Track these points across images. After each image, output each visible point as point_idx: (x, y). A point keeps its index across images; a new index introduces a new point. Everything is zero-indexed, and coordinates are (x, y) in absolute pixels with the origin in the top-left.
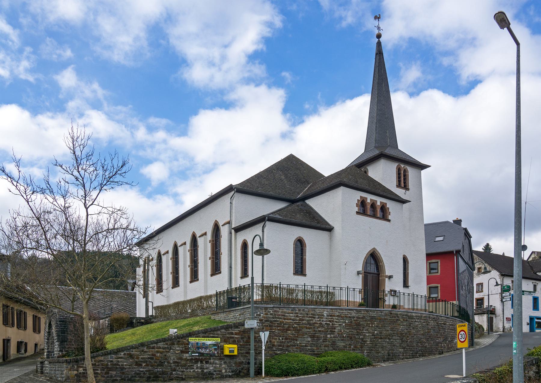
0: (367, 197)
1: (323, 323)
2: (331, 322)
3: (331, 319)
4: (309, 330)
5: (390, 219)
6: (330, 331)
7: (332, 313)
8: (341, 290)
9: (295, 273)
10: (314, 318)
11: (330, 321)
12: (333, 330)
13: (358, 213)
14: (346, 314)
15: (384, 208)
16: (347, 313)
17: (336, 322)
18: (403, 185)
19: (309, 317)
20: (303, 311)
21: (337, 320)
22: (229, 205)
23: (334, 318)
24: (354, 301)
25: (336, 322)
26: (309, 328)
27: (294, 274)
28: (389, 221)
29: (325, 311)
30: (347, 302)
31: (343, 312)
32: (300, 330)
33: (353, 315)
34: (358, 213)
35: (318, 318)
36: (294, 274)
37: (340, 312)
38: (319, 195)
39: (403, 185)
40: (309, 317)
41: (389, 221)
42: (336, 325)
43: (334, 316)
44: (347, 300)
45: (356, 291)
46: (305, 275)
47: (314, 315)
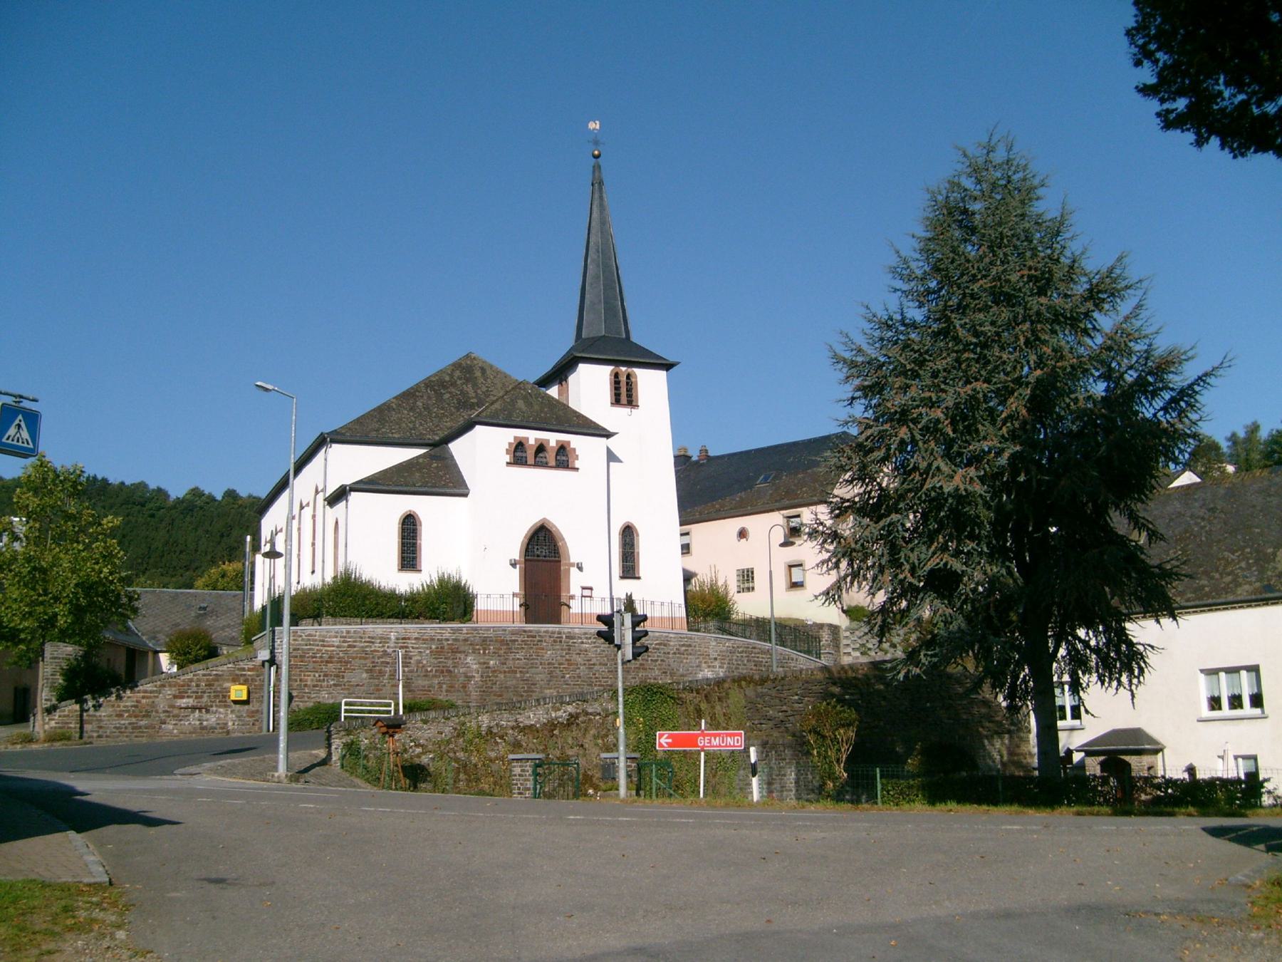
5: (576, 466)
10: (373, 643)
13: (508, 464)
15: (562, 448)
17: (413, 648)
18: (624, 399)
25: (413, 648)
26: (366, 659)
34: (508, 464)
35: (380, 643)
39: (624, 399)
41: (578, 469)
43: (409, 639)
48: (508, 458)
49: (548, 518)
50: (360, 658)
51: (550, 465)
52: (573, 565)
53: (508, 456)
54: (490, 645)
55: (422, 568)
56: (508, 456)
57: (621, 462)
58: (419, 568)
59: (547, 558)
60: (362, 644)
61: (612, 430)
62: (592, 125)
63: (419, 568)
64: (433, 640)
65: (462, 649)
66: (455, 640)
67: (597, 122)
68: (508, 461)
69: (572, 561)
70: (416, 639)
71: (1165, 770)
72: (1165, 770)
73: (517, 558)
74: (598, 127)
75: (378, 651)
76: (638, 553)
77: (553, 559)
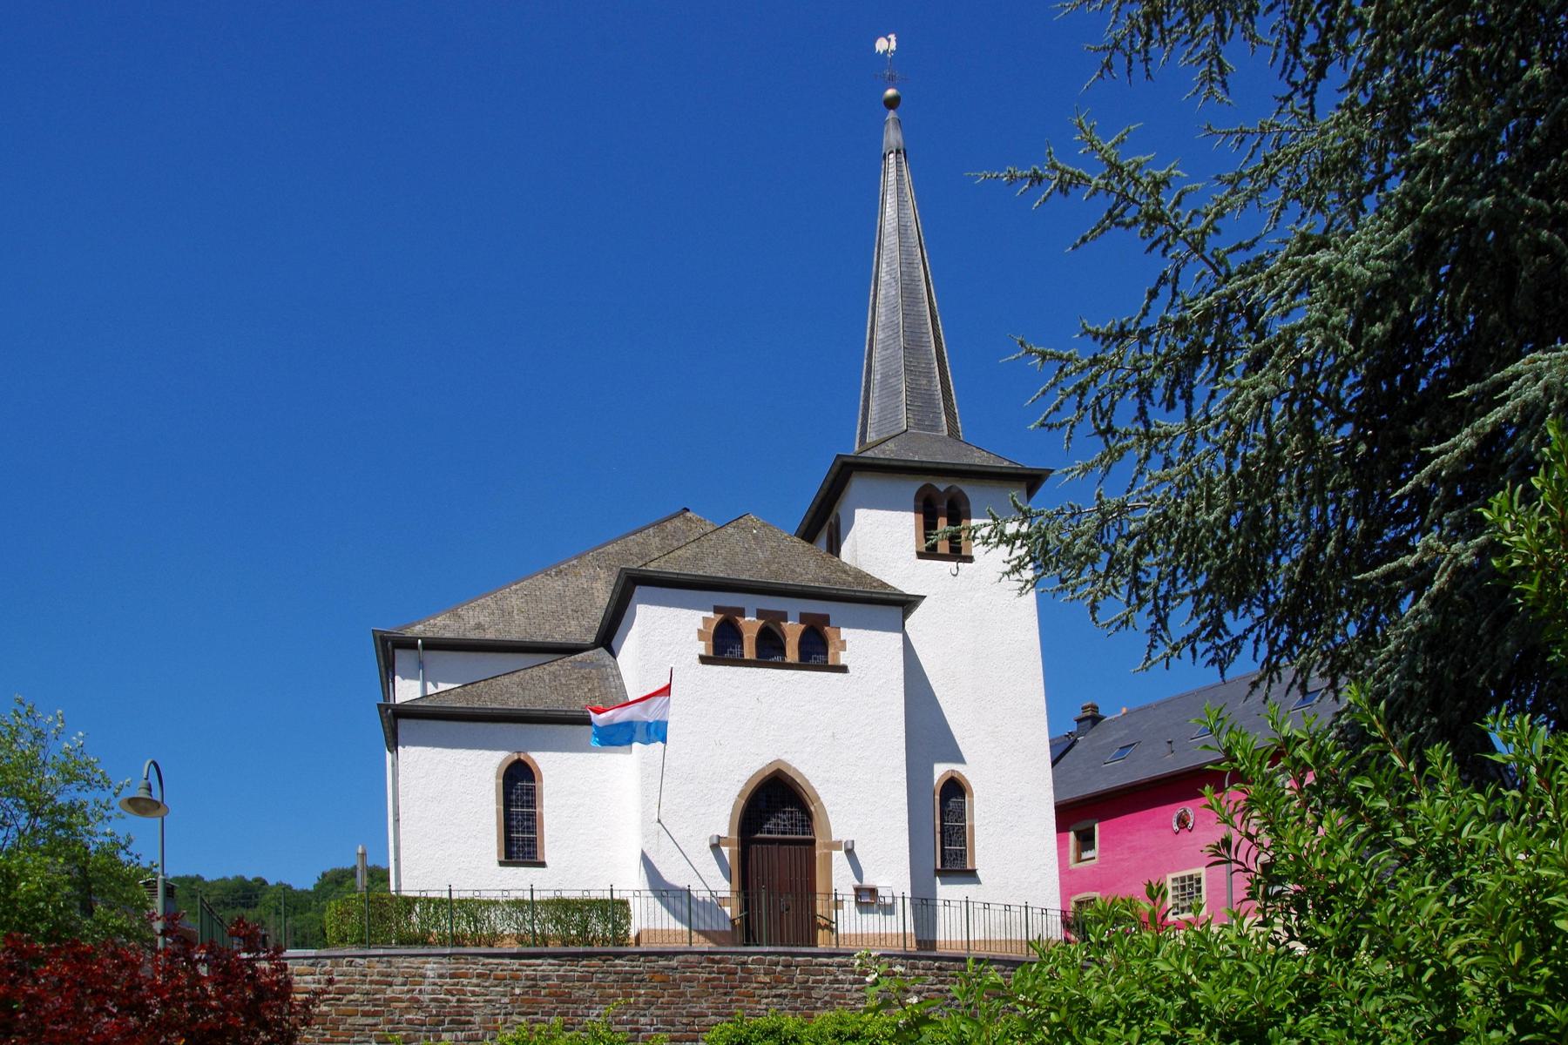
0: (783, 610)
1: (421, 997)
2: (453, 995)
3: (457, 984)
4: (371, 1021)
5: (842, 662)
6: (452, 1022)
7: (457, 969)
8: (987, 911)
9: (503, 859)
10: (390, 984)
11: (449, 992)
12: (463, 1018)
13: (704, 660)
14: (512, 970)
16: (515, 967)
17: (474, 994)
19: (371, 982)
20: (350, 966)
21: (477, 989)
22: (1191, 654)
23: (465, 981)
24: (948, 939)
25: (474, 994)
26: (375, 1014)
27: (502, 864)
28: (843, 669)
29: (429, 963)
30: (901, 937)
31: (501, 964)
32: (335, 1023)
33: (543, 971)
34: (704, 660)
35: (404, 984)
36: (502, 864)
37: (489, 964)
38: (1037, 604)
40: (371, 982)
41: (843, 669)
42: (471, 1002)
43: (465, 976)
44: (965, 938)
45: (992, 912)
46: (543, 865)
47: (389, 976)
48: (702, 648)
49: (786, 758)
50: (365, 1014)
51: (946, 892)
52: (837, 845)
53: (702, 644)
54: (639, 987)
55: (547, 860)
56: (702, 644)
57: (924, 597)
58: (540, 859)
59: (788, 836)
60: (367, 987)
61: (909, 589)
62: (881, 45)
63: (540, 859)
64: (517, 978)
65: (577, 994)
66: (563, 978)
67: (892, 37)
68: (703, 652)
69: (835, 837)
70: (479, 976)
71: (837, 944)
72: (837, 944)
73: (724, 833)
74: (893, 46)
75: (402, 1001)
76: (972, 827)
77: (801, 837)
